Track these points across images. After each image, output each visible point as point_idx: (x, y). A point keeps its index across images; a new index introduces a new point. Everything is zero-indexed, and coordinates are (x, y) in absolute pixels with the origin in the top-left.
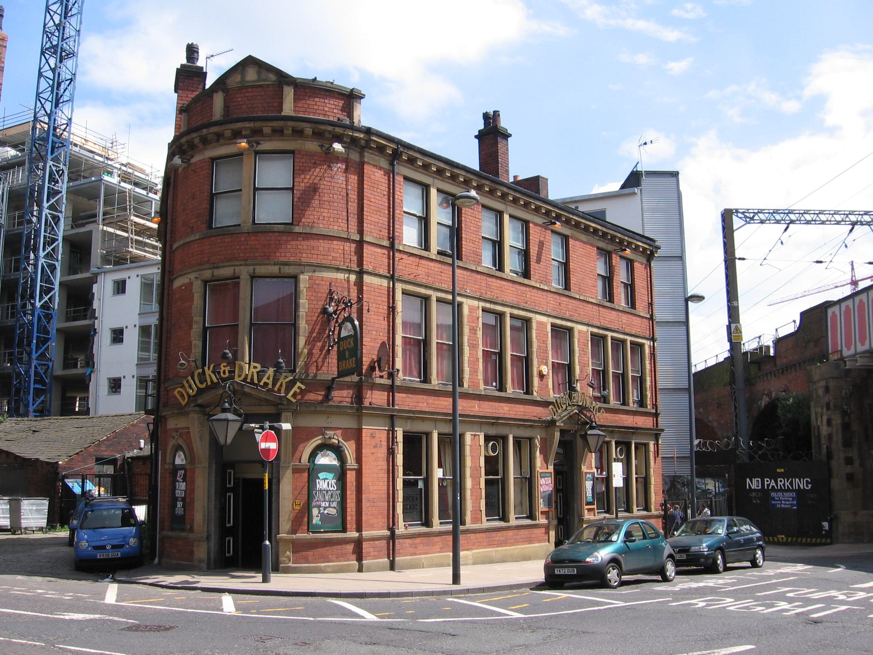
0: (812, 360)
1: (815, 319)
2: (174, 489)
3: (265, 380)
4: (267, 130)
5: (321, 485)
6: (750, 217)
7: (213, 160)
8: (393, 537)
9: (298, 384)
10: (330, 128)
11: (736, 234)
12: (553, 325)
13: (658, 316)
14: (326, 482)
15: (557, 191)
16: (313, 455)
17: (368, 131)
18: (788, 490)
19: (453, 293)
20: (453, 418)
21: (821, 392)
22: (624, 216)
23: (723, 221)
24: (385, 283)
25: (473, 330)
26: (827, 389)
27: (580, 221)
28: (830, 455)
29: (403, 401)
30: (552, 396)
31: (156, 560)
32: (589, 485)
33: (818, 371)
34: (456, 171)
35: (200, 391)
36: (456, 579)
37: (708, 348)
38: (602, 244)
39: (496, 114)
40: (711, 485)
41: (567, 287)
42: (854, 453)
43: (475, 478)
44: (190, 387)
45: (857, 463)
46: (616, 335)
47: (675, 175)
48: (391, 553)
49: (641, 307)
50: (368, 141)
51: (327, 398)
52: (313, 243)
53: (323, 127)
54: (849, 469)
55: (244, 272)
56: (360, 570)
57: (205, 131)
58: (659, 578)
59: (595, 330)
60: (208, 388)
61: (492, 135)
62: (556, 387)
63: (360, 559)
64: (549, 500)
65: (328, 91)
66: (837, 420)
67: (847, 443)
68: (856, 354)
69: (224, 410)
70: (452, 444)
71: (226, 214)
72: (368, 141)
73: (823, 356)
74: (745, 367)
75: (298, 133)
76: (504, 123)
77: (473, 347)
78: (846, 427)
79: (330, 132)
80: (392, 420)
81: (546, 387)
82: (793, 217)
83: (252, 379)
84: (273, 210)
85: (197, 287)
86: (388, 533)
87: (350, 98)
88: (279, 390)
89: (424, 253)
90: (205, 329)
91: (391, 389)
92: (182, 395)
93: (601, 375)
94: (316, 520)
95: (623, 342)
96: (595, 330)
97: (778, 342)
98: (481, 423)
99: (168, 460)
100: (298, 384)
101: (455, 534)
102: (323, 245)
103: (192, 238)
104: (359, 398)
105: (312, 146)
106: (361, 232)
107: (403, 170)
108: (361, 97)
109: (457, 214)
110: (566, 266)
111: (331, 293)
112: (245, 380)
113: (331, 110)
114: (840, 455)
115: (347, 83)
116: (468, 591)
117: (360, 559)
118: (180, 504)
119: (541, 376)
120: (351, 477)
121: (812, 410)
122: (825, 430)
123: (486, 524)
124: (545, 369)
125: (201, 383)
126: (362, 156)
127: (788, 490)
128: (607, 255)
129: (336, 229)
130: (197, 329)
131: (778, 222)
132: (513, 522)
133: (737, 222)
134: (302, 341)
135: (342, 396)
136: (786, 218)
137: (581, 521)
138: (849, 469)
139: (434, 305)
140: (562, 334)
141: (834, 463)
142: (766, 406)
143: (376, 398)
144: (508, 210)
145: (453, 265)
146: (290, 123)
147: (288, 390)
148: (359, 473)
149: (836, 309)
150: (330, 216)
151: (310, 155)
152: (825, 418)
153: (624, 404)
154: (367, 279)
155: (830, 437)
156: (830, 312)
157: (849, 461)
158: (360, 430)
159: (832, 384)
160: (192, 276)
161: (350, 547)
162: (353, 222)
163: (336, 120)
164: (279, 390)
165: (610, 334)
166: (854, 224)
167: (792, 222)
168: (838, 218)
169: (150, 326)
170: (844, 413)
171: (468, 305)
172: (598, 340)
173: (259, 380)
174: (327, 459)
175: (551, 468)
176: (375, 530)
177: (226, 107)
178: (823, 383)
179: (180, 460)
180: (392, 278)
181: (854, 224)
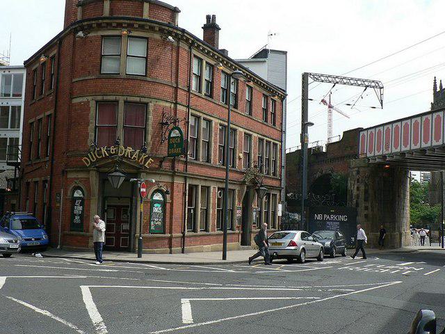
0: (349, 157)
1: (352, 136)
2: (73, 209)
3: (134, 156)
4: (136, 26)
5: (155, 210)
6: (317, 78)
7: (102, 36)
8: (184, 237)
9: (151, 159)
10: (167, 28)
11: (309, 86)
12: (245, 133)
13: (171, 90)
14: (157, 209)
15: (231, 55)
16: (153, 195)
17: (183, 31)
18: (336, 221)
19: (228, 122)
20: (226, 181)
21: (354, 173)
22: (261, 71)
23: (303, 79)
24: (185, 109)
25: (216, 134)
26: (358, 172)
27: (236, 70)
28: (357, 205)
29: (191, 170)
30: (243, 169)
31: (59, 247)
32: (254, 213)
33: (353, 162)
34: (153, 24)
35: (98, 160)
36: (224, 257)
37: (292, 143)
38: (265, 92)
39: (214, 16)
40: (297, 217)
41: (250, 114)
42: (369, 205)
43: (214, 209)
44: (92, 157)
45: (370, 210)
46: (268, 139)
47: (285, 53)
48: (183, 245)
49: (278, 123)
50: (183, 36)
51: (160, 166)
52: (156, 87)
53: (163, 27)
54: (366, 212)
55: (121, 99)
56: (171, 253)
57: (100, 21)
58: (341, 255)
59: (260, 136)
60: (103, 158)
61: (211, 27)
62: (245, 166)
63: (170, 247)
64: (239, 220)
65: (166, 8)
66: (362, 188)
67: (366, 200)
68: (374, 156)
69: (116, 171)
70: (206, 190)
71: (109, 66)
72: (183, 36)
73: (356, 156)
74: (309, 157)
75: (152, 29)
76: (218, 22)
77: (215, 143)
78: (366, 192)
79: (167, 30)
80: (185, 178)
81: (240, 165)
82: (337, 80)
83: (128, 155)
84: (135, 68)
85: (92, 104)
86: (182, 235)
87: (174, 11)
88: (141, 161)
89: (199, 94)
90: (96, 127)
91: (186, 163)
92: (86, 160)
93: (261, 158)
94: (152, 228)
95: (270, 142)
96: (260, 136)
97: (329, 145)
98: (217, 181)
99: (69, 193)
100: (151, 159)
101: (225, 235)
102: (160, 88)
103: (90, 77)
104: (173, 167)
105: (157, 36)
106: (177, 83)
107: (194, 52)
108: (180, 12)
109: (212, 74)
110: (250, 103)
111: (163, 114)
112: (124, 155)
113: (164, 18)
114: (362, 205)
115: (174, 4)
116: (230, 263)
117: (170, 247)
118: (77, 218)
119: (240, 159)
120: (168, 206)
121: (349, 182)
122: (355, 192)
123: (217, 232)
124: (241, 155)
125: (99, 155)
126: (178, 43)
127: (336, 221)
128: (266, 97)
129: (167, 80)
130: (92, 127)
131: (330, 82)
132: (199, 233)
133: (310, 80)
134: (149, 137)
135: (166, 165)
136: (336, 80)
137: (251, 232)
138: (366, 212)
139: (202, 120)
140: (248, 136)
141: (359, 209)
142: (319, 177)
143: (180, 167)
144: (206, 59)
145: (229, 109)
146: (148, 23)
147: (145, 163)
148: (172, 204)
149: (365, 133)
150: (163, 74)
151: (156, 41)
152: (356, 186)
153: (196, 159)
154: (178, 106)
155: (358, 196)
156: (361, 134)
157: (366, 208)
158: (173, 183)
159: (361, 170)
160: (90, 98)
161: (166, 241)
162: (174, 77)
163: (167, 23)
164: (141, 161)
165: (265, 138)
166: (367, 87)
167: (337, 83)
168: (359, 83)
169: (9, 107)
170: (366, 185)
171: (215, 121)
172: (261, 140)
173: (131, 156)
174: (158, 197)
175: (241, 206)
176: (177, 234)
177: (111, 10)
178: (356, 169)
179: (78, 194)
180: (188, 107)
181: (367, 87)
